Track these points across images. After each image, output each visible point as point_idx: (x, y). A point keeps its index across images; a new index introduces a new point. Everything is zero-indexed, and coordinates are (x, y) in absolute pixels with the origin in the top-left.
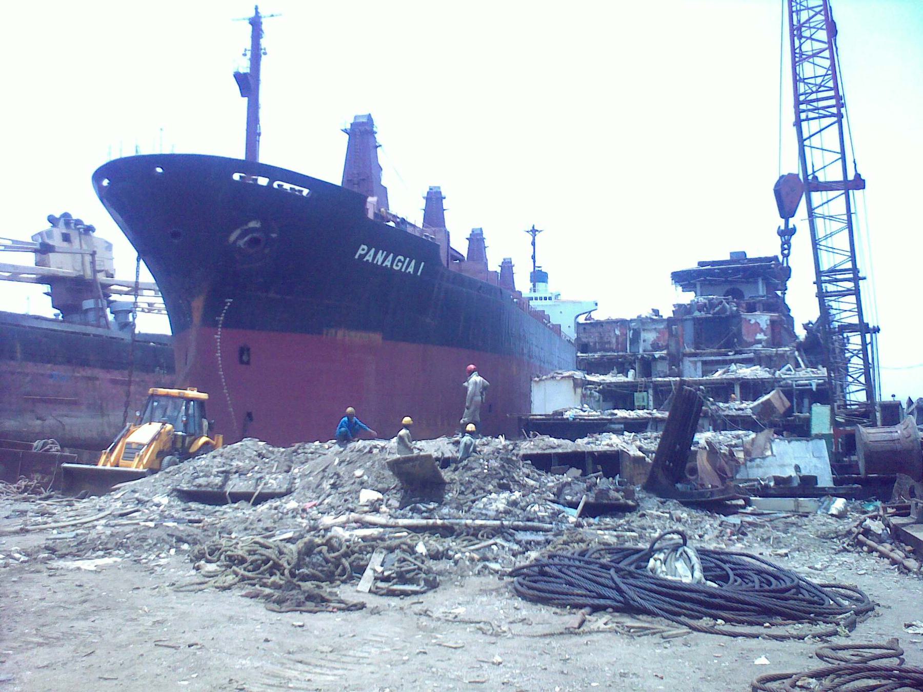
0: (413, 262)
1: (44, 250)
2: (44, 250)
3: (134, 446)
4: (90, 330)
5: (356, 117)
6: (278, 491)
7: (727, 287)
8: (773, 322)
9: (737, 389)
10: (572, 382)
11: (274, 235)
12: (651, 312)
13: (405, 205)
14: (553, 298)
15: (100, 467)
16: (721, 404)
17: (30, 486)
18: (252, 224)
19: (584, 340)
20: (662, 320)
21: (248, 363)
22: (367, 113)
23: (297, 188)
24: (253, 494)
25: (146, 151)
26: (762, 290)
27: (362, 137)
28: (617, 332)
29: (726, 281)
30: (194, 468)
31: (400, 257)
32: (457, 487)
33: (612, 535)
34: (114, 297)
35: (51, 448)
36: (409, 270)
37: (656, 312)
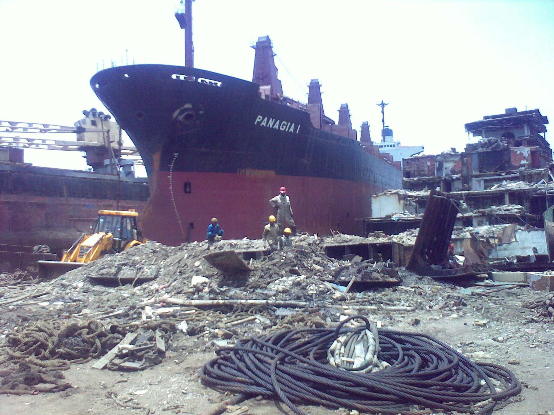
0: (293, 125)
1: (80, 130)
2: (80, 130)
3: (85, 248)
4: (107, 177)
5: (259, 38)
6: (150, 277)
7: (504, 132)
8: (533, 153)
9: (507, 198)
10: (397, 196)
11: (201, 112)
12: (450, 150)
13: (295, 91)
14: (396, 145)
15: (62, 262)
16: (494, 207)
17: (23, 275)
18: (187, 106)
19: (408, 170)
20: (457, 154)
21: (190, 192)
22: (266, 35)
23: (213, 82)
24: (134, 279)
25: (118, 64)
26: (527, 132)
27: (264, 50)
28: (429, 164)
29: (502, 128)
30: (103, 263)
31: (284, 122)
32: (259, 273)
33: (354, 309)
34: (123, 157)
35: (43, 250)
36: (275, 126)
37: (454, 150)
